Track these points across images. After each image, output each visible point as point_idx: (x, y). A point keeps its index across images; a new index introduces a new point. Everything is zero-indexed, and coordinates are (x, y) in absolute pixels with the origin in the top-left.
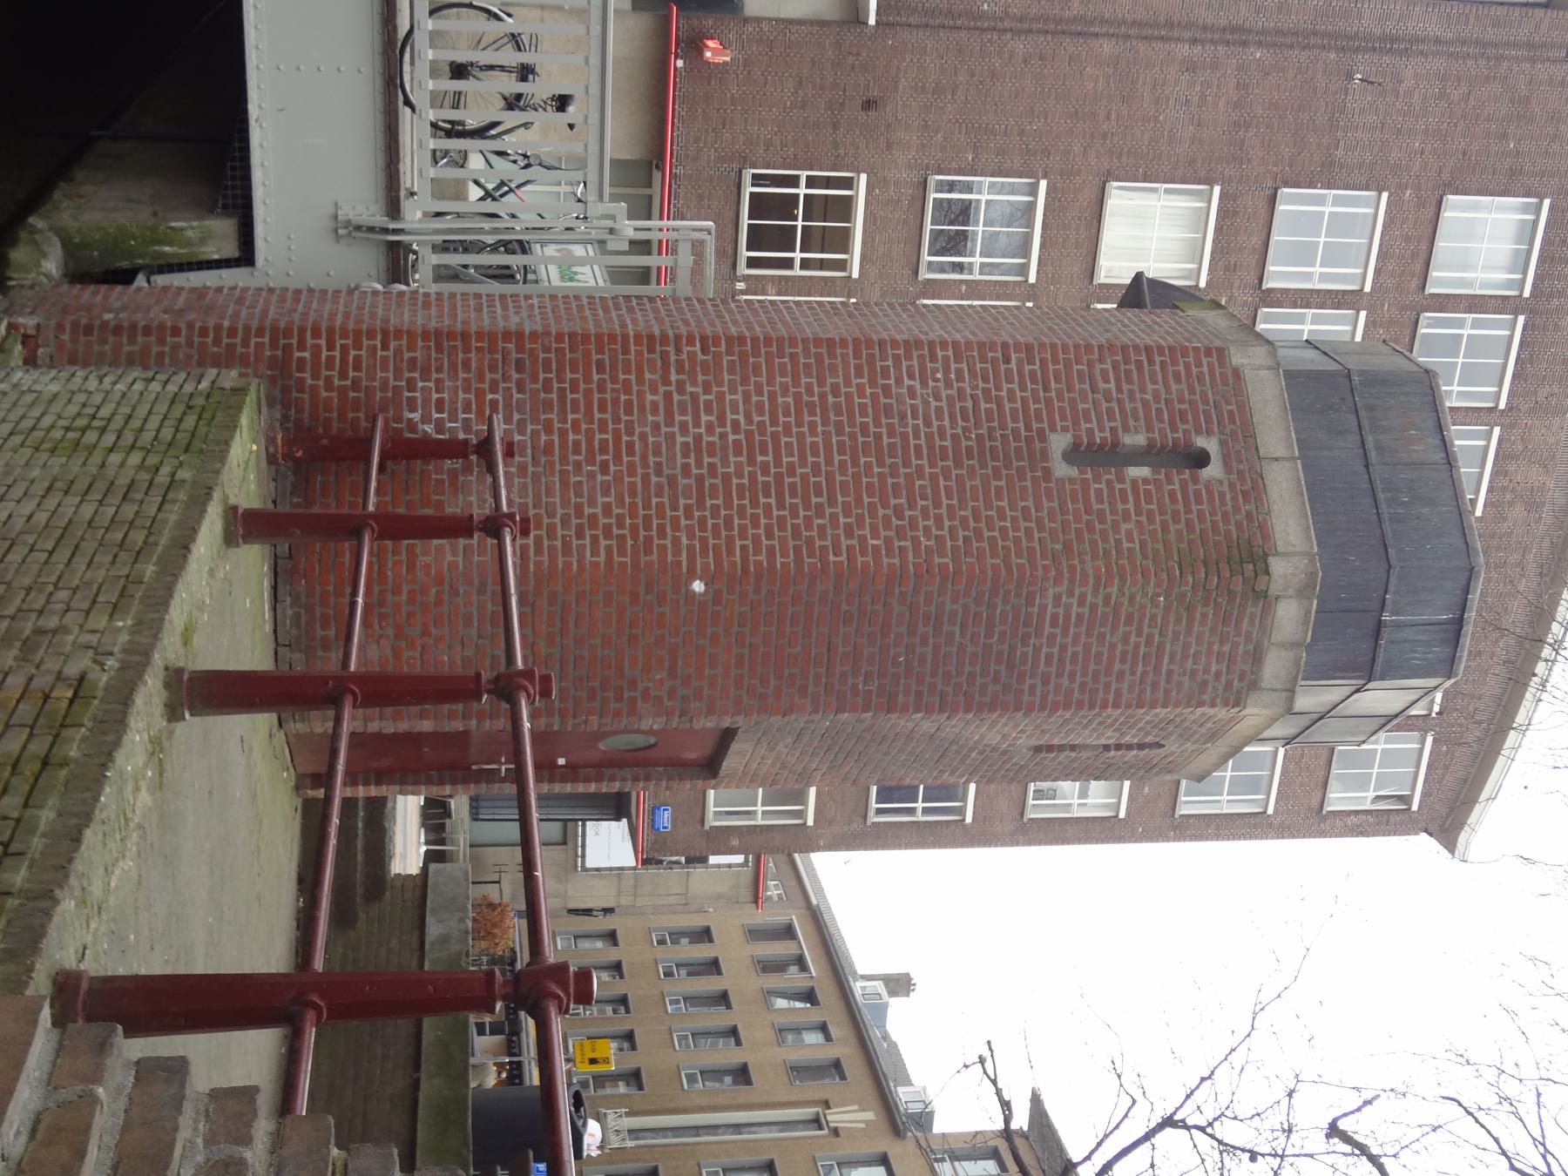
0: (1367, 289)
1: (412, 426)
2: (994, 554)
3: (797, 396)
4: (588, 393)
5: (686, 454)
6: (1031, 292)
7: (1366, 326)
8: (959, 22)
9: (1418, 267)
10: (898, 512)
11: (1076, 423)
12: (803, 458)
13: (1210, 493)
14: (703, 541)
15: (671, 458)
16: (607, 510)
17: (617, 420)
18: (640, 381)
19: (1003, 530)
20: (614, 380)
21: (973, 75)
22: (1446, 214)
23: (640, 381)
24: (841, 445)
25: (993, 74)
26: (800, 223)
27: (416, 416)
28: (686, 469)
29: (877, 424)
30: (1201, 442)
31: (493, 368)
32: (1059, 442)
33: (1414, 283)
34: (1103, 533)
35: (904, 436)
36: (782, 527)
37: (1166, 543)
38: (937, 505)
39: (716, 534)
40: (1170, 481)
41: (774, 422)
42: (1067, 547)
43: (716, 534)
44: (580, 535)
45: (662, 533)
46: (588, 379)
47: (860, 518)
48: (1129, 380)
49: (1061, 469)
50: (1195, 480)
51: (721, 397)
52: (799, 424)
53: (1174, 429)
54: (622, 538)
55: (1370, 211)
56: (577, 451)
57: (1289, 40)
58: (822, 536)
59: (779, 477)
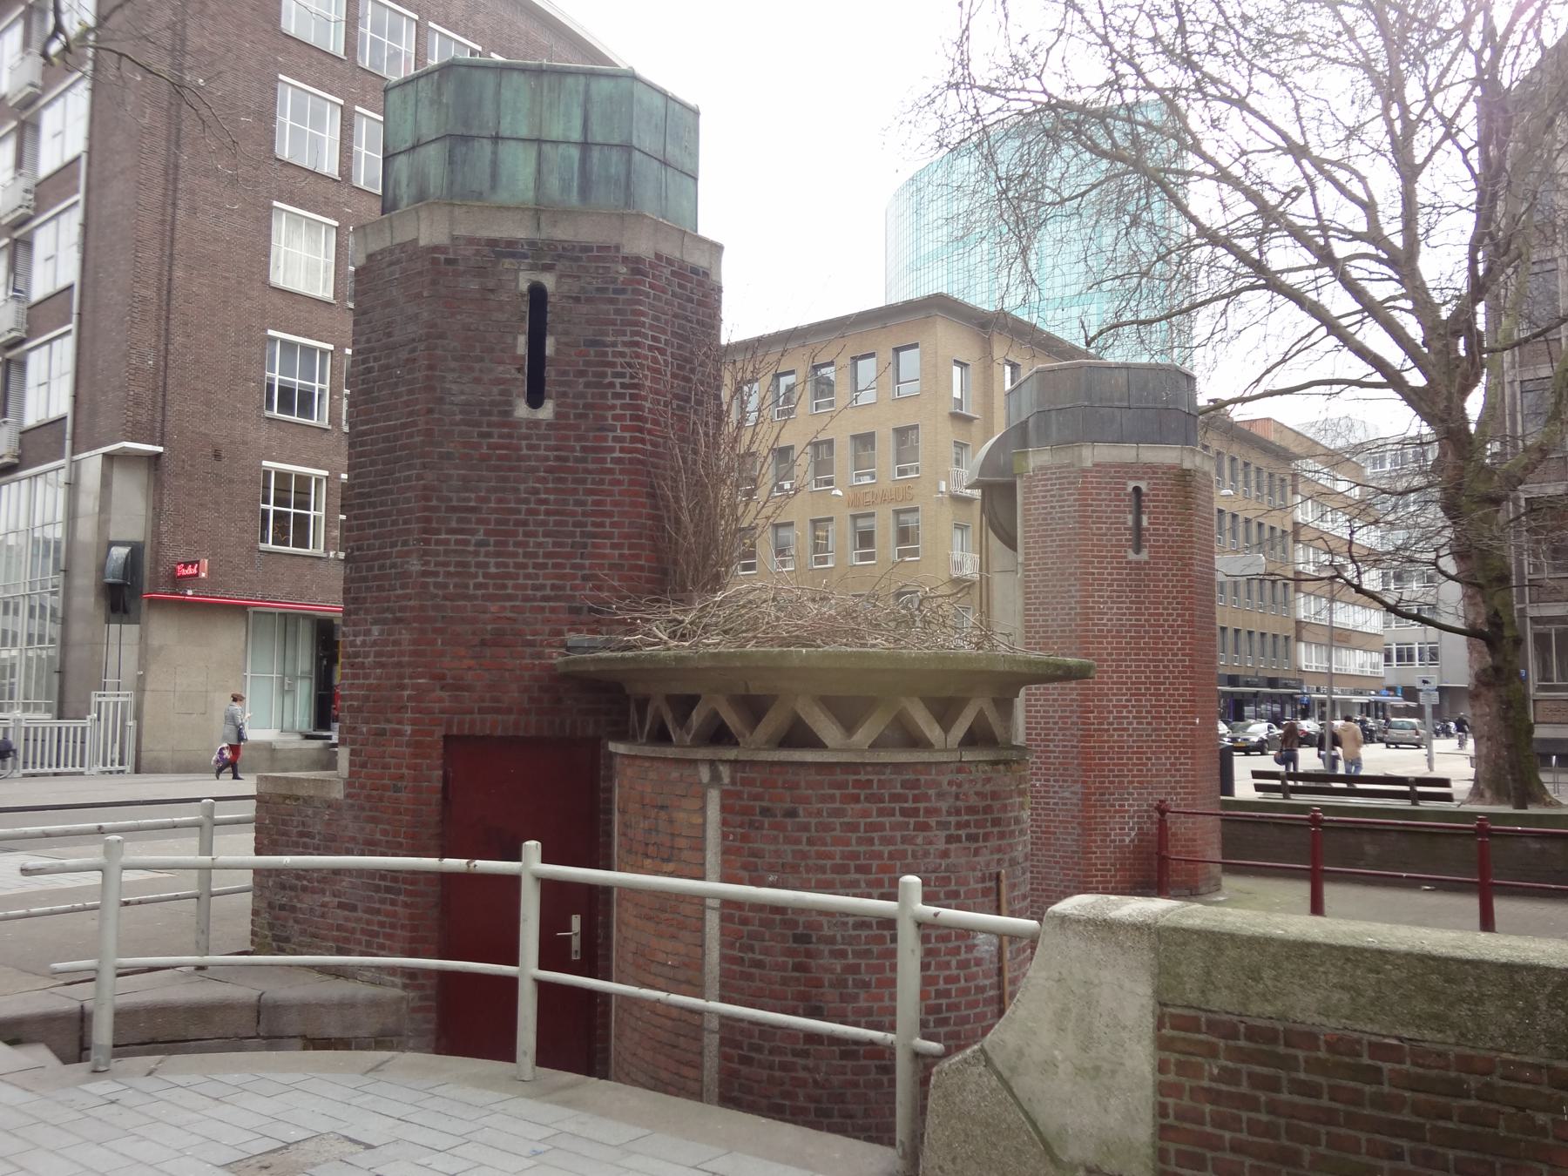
0: (341, 102)
1: (1132, 841)
2: (1184, 592)
3: (1113, 672)
4: (1114, 765)
5: (1142, 723)
6: (339, 348)
7: (364, 107)
8: (161, 384)
9: (328, 61)
10: (1165, 632)
11: (1123, 546)
12: (1142, 672)
13: (1154, 489)
14: (1180, 718)
15: (1144, 729)
16: (1167, 758)
17: (1127, 753)
18: (1108, 741)
19: (1173, 586)
20: (1108, 753)
21: (198, 377)
22: (292, 31)
23: (1108, 741)
24: (1136, 654)
25: (197, 361)
26: (292, 510)
27: (1127, 840)
28: (1148, 723)
29: (1125, 637)
30: (1130, 489)
31: (1104, 806)
32: (1132, 556)
33: (339, 66)
34: (1173, 541)
35: (1131, 625)
36: (1174, 684)
37: (1178, 514)
38: (1162, 614)
39: (1178, 712)
40: (1148, 507)
41: (1126, 683)
42: (1180, 559)
43: (1178, 712)
44: (1179, 770)
45: (1178, 736)
46: (1108, 765)
47: (1170, 649)
48: (1101, 517)
49: (1144, 556)
50: (1147, 495)
51: (1115, 706)
52: (1126, 672)
53: (1124, 500)
54: (1181, 753)
55: (290, 89)
56: (1141, 770)
57: (174, 131)
58: (1177, 667)
59: (1151, 683)
